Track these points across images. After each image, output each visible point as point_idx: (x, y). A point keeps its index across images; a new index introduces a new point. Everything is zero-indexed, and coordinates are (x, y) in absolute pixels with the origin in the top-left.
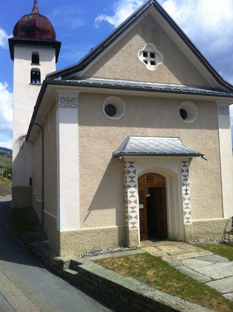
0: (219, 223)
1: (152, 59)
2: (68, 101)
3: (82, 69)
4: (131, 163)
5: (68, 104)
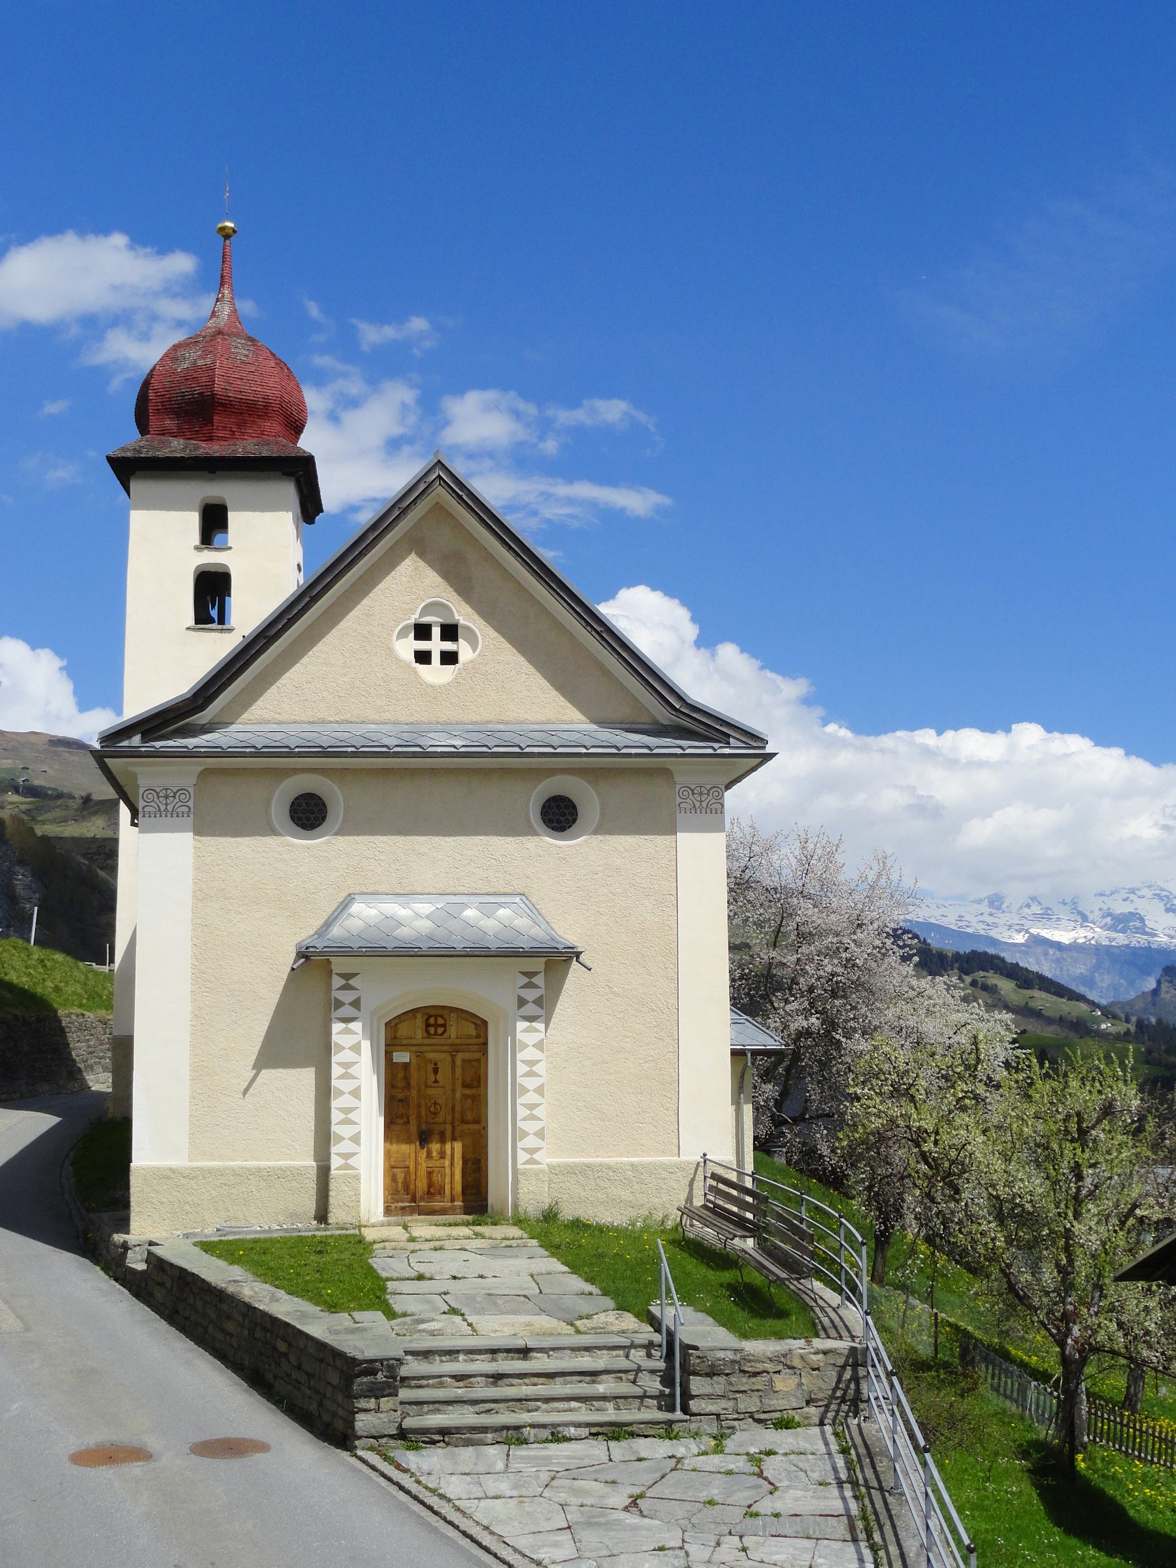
0: (659, 1174)
1: (449, 646)
2: (167, 797)
3: (202, 708)
4: (348, 976)
5: (166, 804)
